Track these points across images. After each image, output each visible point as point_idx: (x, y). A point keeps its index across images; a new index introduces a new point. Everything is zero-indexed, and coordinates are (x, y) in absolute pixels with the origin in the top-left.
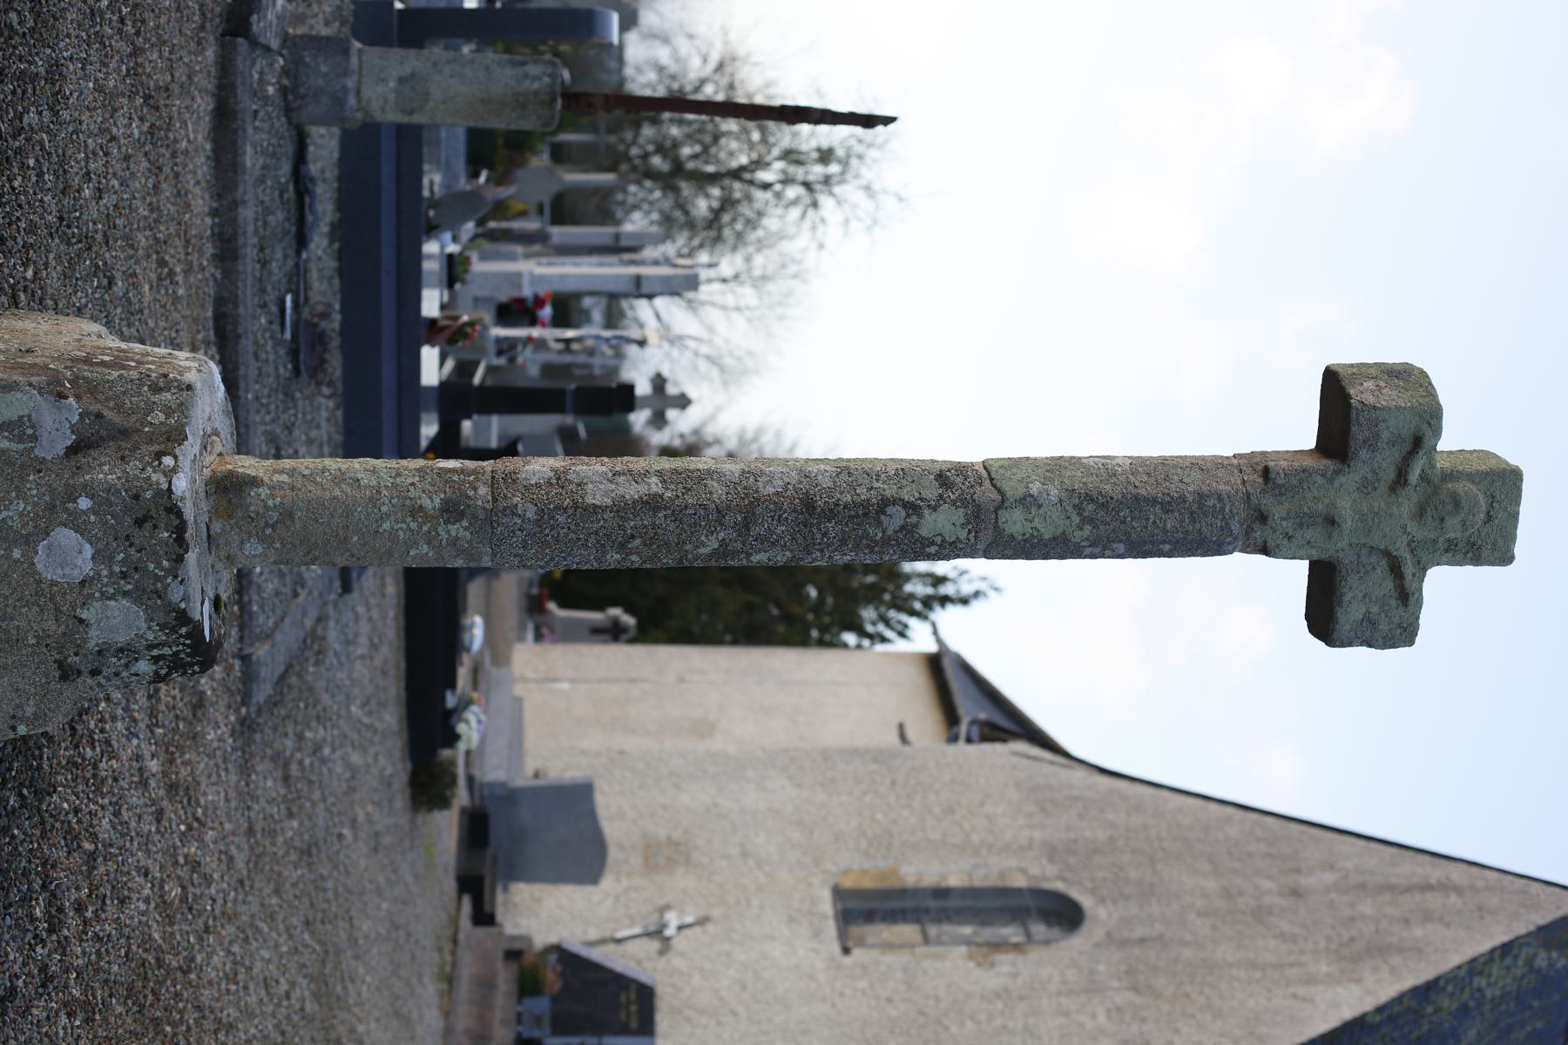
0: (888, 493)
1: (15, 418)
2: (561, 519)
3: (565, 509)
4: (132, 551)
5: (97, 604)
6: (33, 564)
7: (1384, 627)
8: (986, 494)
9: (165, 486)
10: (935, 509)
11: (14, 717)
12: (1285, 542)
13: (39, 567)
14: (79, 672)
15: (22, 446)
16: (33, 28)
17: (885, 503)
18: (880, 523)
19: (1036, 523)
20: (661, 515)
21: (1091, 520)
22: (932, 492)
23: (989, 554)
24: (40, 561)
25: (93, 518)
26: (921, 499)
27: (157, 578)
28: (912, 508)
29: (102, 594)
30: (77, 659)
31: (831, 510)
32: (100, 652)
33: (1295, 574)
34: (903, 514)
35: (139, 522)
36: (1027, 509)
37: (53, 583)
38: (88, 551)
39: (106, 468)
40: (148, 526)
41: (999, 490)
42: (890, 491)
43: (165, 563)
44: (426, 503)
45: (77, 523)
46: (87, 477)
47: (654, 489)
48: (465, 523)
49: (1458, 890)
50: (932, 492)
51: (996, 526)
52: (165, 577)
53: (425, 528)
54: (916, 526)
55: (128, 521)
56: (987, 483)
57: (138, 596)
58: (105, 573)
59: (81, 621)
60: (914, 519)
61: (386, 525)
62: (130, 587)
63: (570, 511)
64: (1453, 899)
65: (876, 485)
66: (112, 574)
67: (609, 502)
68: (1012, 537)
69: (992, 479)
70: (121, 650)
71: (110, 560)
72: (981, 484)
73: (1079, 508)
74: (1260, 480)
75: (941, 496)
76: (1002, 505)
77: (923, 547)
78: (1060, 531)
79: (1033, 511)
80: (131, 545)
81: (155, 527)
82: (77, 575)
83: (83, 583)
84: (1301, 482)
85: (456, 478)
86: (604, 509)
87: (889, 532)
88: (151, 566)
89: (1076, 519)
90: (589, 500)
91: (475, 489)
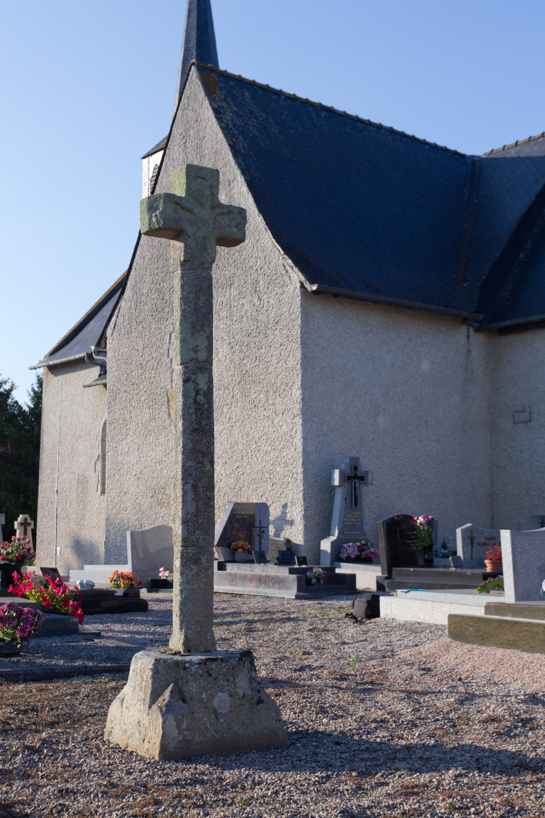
0: (192, 401)
1: (175, 722)
2: (200, 521)
3: (197, 520)
4: (220, 677)
5: (238, 690)
6: (225, 714)
7: (239, 220)
8: (191, 366)
9: (197, 666)
10: (198, 384)
11: (276, 720)
12: (210, 255)
13: (226, 711)
14: (259, 697)
15: (185, 720)
16: (298, 703)
17: (196, 402)
18: (202, 404)
19: (203, 347)
20: (199, 484)
21: (202, 327)
22: (191, 385)
23: (211, 364)
24: (224, 712)
25: (209, 692)
26: (194, 389)
27: (228, 669)
28: (197, 392)
29: (234, 688)
30: (255, 698)
31: (198, 422)
32: (252, 690)
33: (222, 251)
34: (200, 396)
35: (210, 675)
36: (198, 350)
37: (231, 707)
38: (220, 694)
39: (191, 688)
40: (211, 672)
41: (191, 360)
42: (191, 400)
43: (224, 665)
44: (195, 570)
45: (211, 698)
46: (195, 695)
47: (190, 487)
48: (201, 557)
49: (187, 131)
50: (191, 385)
51: (204, 362)
52: (228, 665)
53: (203, 571)
54: (203, 391)
55: (209, 679)
56: (188, 365)
57: (235, 677)
58: (227, 688)
59: (243, 696)
60: (201, 392)
61: (202, 586)
62: (232, 678)
63: (198, 518)
64: (191, 133)
65: (188, 405)
66: (227, 685)
67: (194, 504)
68: (207, 357)
69: (186, 363)
70: (250, 682)
71: (223, 686)
72: (188, 367)
73: (198, 331)
74: (188, 263)
75: (193, 382)
76: (197, 360)
77: (210, 389)
78: (206, 339)
79: (198, 348)
80: (218, 678)
81: (211, 669)
82: (228, 698)
83: (231, 696)
84: (190, 248)
85: (184, 560)
86: (197, 506)
87: (206, 401)
88: (225, 670)
89: (202, 333)
90: (194, 511)
91: (189, 553)
